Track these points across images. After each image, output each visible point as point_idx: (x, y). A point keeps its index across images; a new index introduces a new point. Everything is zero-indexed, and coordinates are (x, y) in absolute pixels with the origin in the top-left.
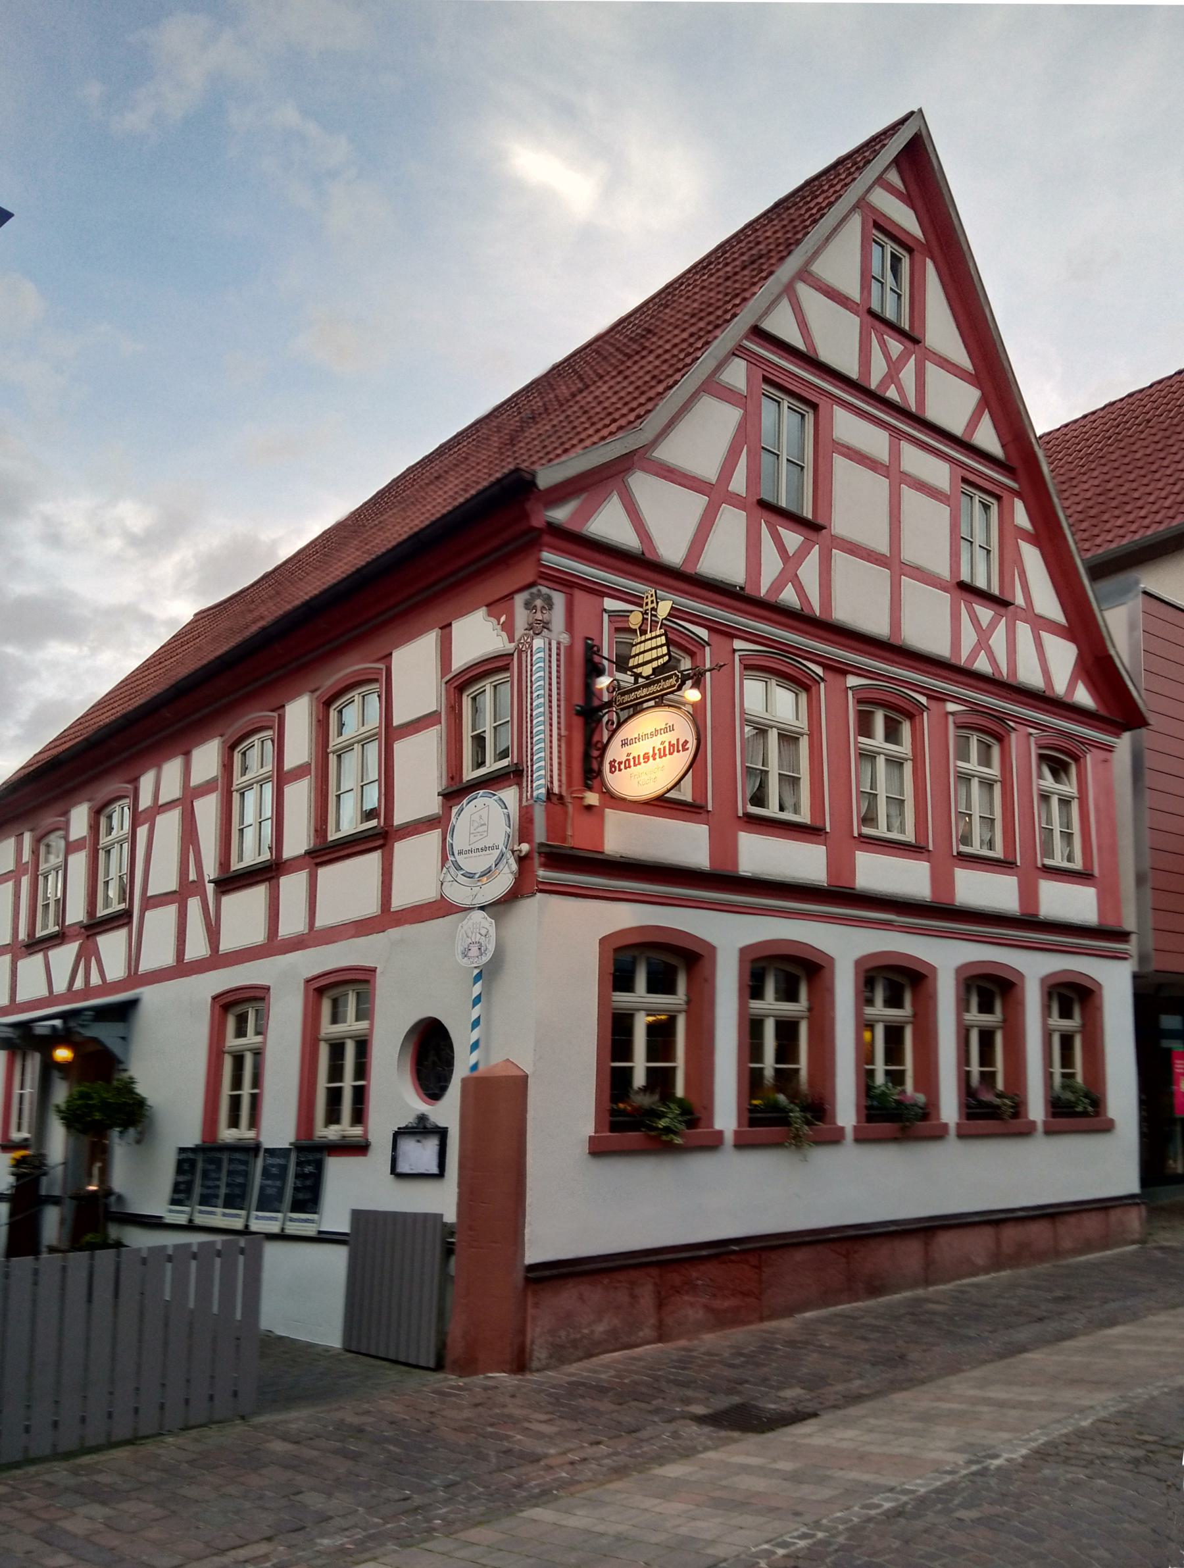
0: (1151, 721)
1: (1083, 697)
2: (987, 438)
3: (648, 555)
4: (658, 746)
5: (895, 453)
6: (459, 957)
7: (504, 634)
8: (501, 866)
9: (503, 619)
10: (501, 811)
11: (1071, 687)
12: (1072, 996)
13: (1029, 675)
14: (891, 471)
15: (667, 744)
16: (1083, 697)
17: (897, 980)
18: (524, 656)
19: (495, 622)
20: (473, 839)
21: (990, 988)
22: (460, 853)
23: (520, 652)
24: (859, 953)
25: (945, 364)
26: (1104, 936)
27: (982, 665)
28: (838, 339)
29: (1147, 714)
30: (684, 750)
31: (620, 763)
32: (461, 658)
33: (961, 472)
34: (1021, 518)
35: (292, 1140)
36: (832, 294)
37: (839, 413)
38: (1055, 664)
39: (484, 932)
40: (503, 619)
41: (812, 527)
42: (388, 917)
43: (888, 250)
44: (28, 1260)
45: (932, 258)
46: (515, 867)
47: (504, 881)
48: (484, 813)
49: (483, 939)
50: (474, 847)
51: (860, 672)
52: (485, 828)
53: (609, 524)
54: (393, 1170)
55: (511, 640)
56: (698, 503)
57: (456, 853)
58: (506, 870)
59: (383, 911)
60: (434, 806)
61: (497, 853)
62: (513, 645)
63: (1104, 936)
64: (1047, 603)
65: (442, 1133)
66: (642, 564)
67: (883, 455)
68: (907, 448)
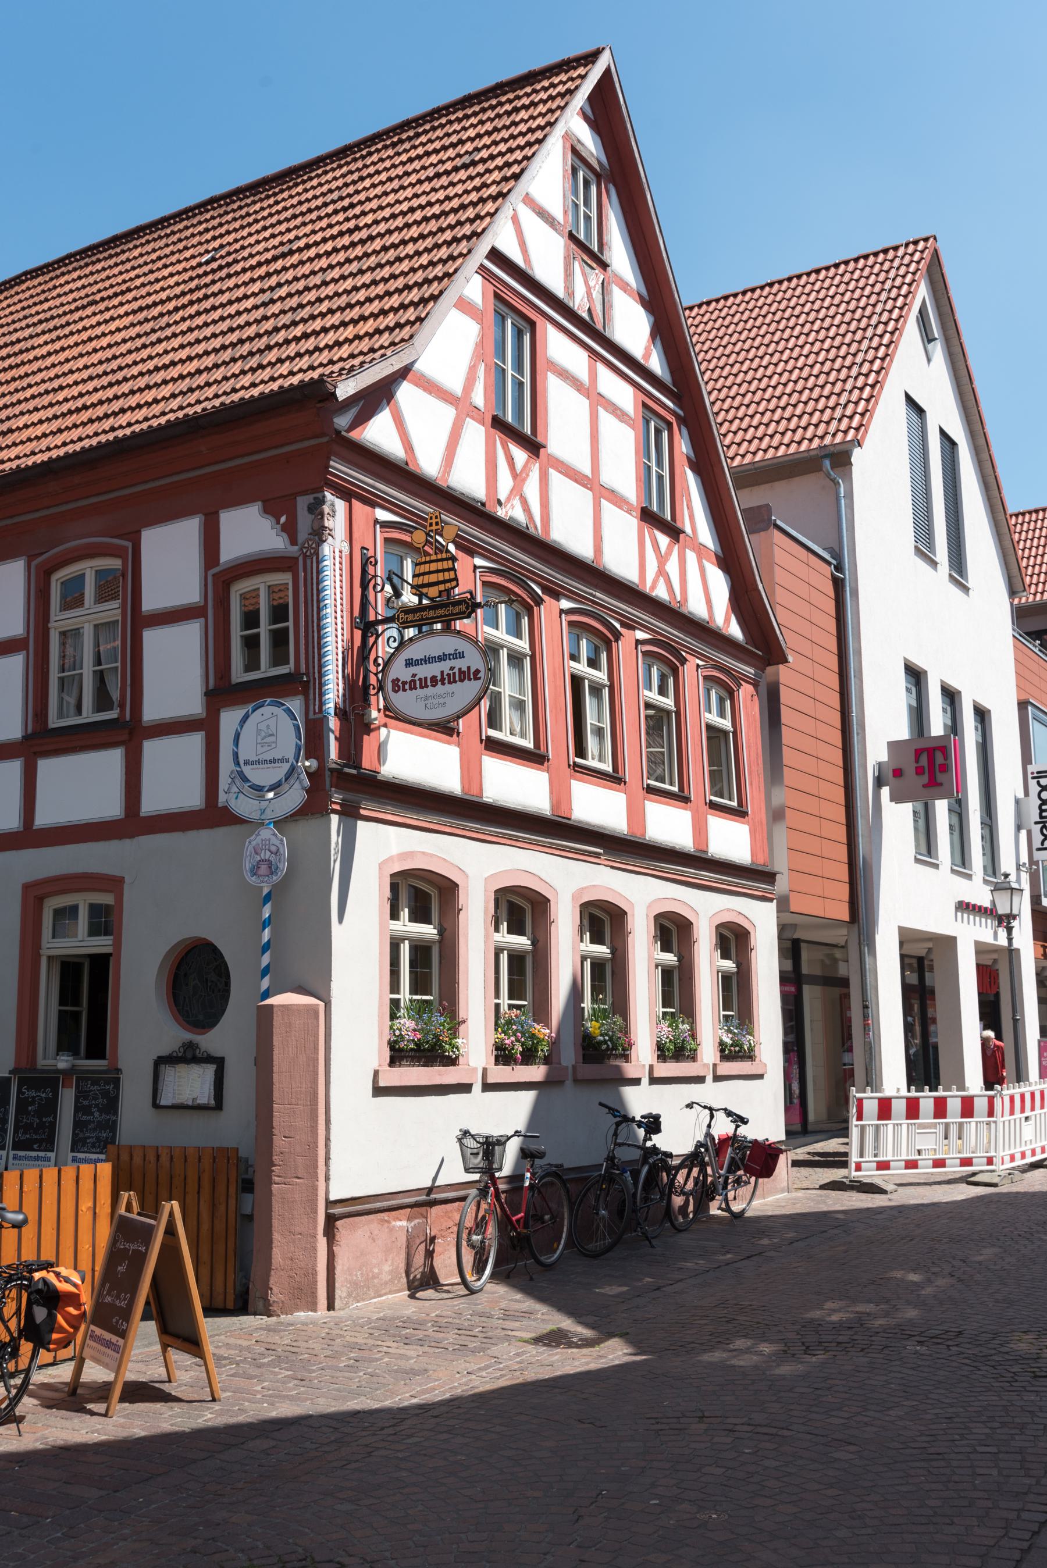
0: (790, 659)
1: (735, 631)
2: (656, 364)
3: (412, 467)
4: (447, 671)
5: (593, 374)
6: (247, 876)
7: (285, 535)
8: (292, 781)
9: (283, 519)
10: (290, 723)
11: (727, 621)
12: (733, 940)
13: (696, 607)
14: (589, 391)
15: (456, 670)
16: (735, 631)
17: (520, 908)
18: (309, 562)
19: (273, 520)
20: (260, 750)
21: (673, 930)
22: (246, 763)
23: (305, 556)
24: (574, 887)
25: (624, 286)
26: (753, 877)
27: (661, 593)
28: (548, 260)
29: (787, 651)
30: (476, 678)
31: (404, 683)
32: (231, 551)
33: (642, 397)
34: (683, 447)
35: (11, 1065)
36: (543, 214)
37: (552, 332)
38: (708, 595)
39: (273, 849)
40: (283, 519)
41: (533, 446)
42: (133, 822)
43: (581, 174)
44: (250, 1196)
45: (615, 185)
46: (307, 783)
47: (295, 796)
48: (272, 722)
49: (273, 858)
50: (262, 757)
51: (572, 596)
52: (273, 739)
53: (379, 433)
54: (156, 1105)
55: (293, 541)
56: (449, 413)
57: (242, 763)
58: (297, 785)
59: (127, 815)
60: (193, 705)
61: (286, 767)
62: (296, 548)
63: (753, 877)
64: (706, 535)
65: (219, 1063)
66: (401, 474)
67: (584, 376)
68: (601, 369)
